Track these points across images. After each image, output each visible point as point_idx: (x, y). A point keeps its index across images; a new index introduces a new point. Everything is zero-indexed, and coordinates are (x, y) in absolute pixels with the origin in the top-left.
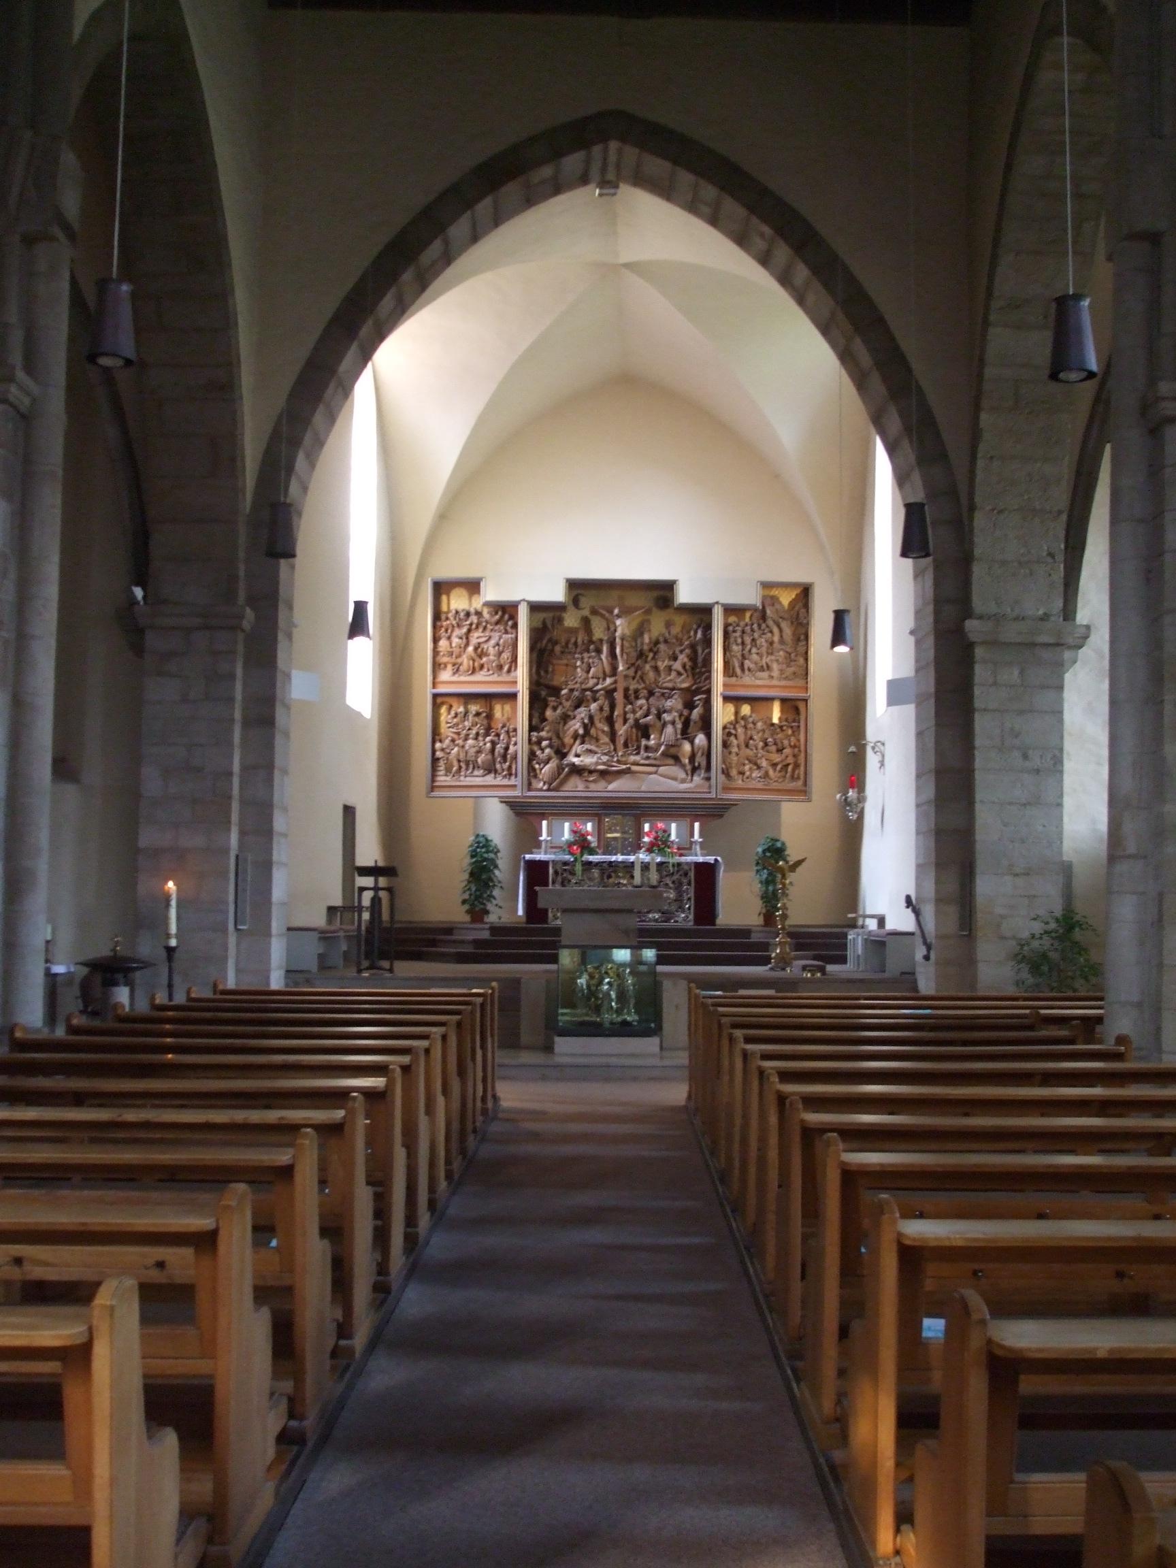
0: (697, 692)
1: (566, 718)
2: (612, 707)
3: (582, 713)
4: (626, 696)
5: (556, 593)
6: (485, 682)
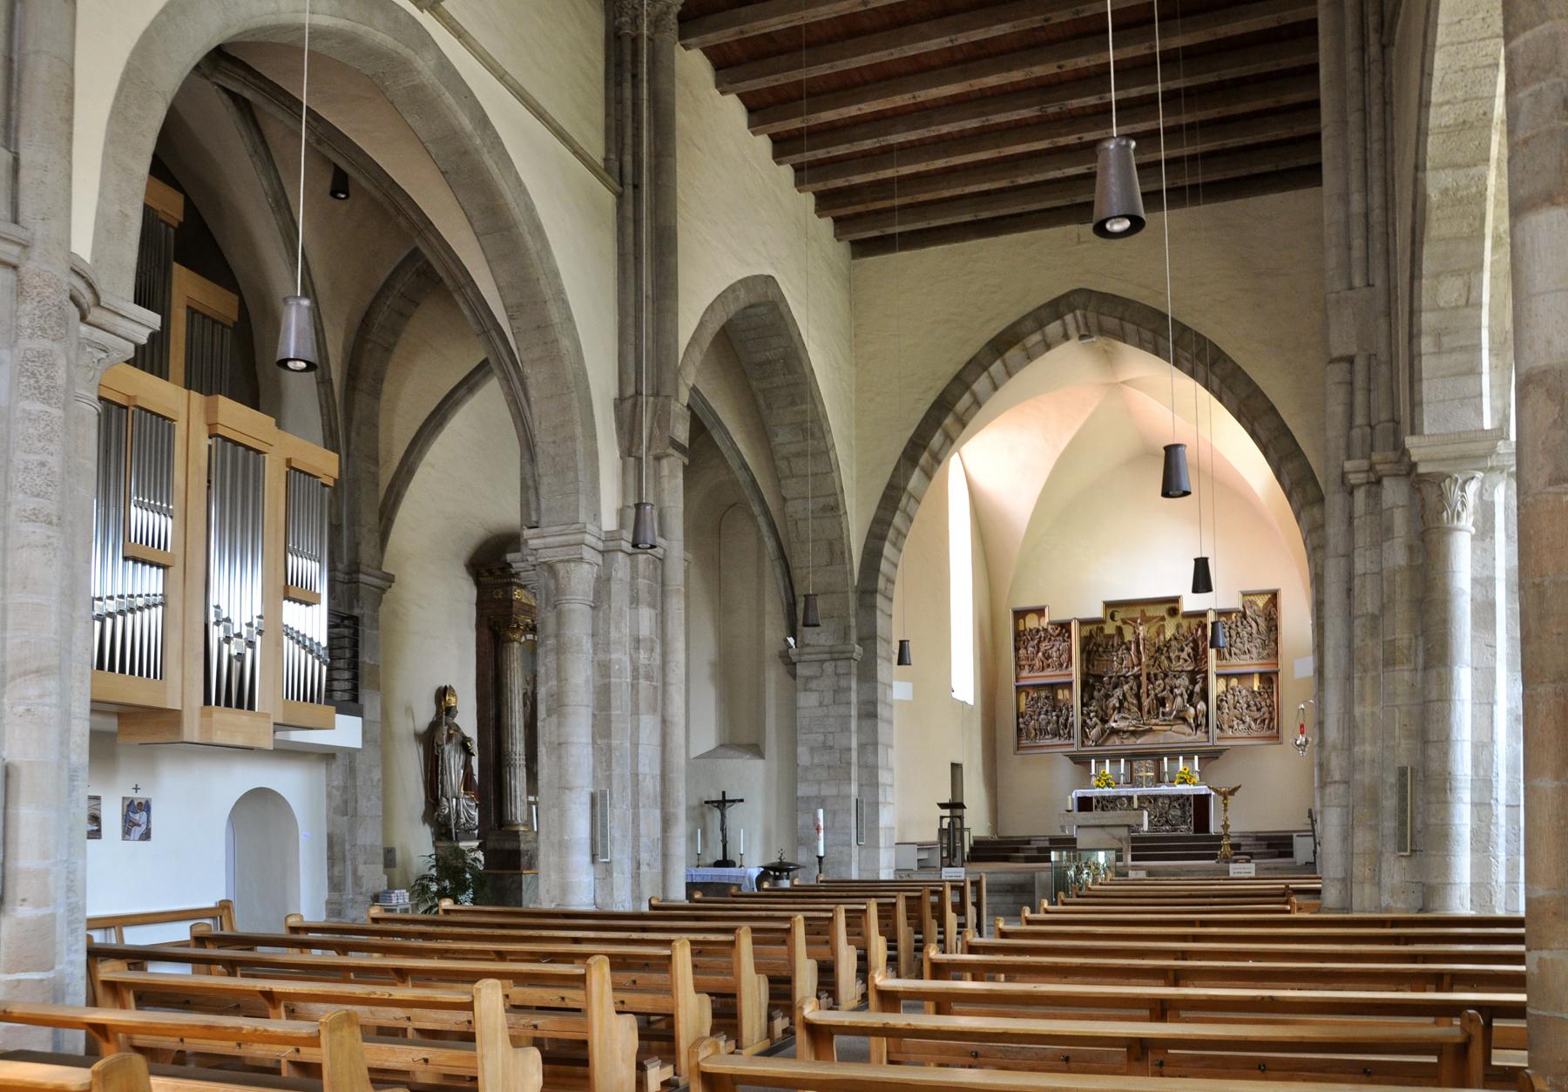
0: (1199, 672)
1: (1107, 697)
2: (1139, 687)
3: (1118, 692)
4: (1148, 678)
5: (1098, 612)
6: (1050, 676)
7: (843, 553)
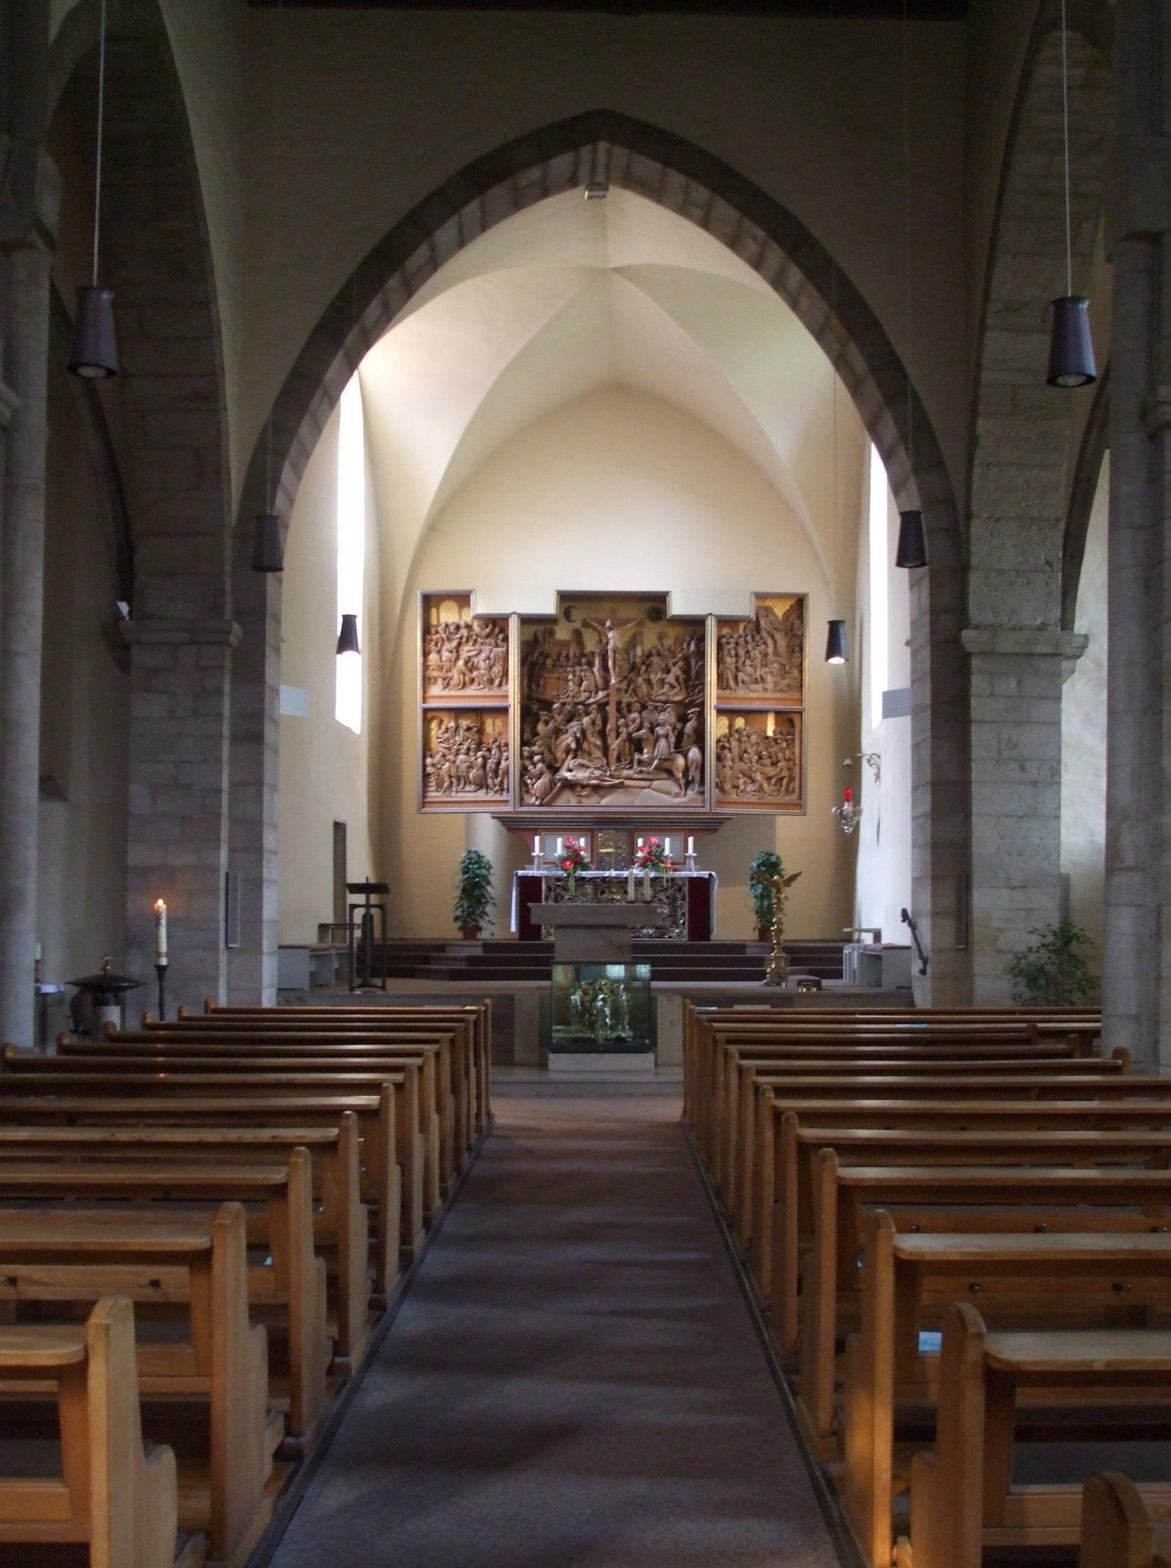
1: (558, 732)
2: (605, 721)
3: (574, 727)
4: (619, 710)
5: (547, 606)
6: (475, 696)
7: (218, 472)
